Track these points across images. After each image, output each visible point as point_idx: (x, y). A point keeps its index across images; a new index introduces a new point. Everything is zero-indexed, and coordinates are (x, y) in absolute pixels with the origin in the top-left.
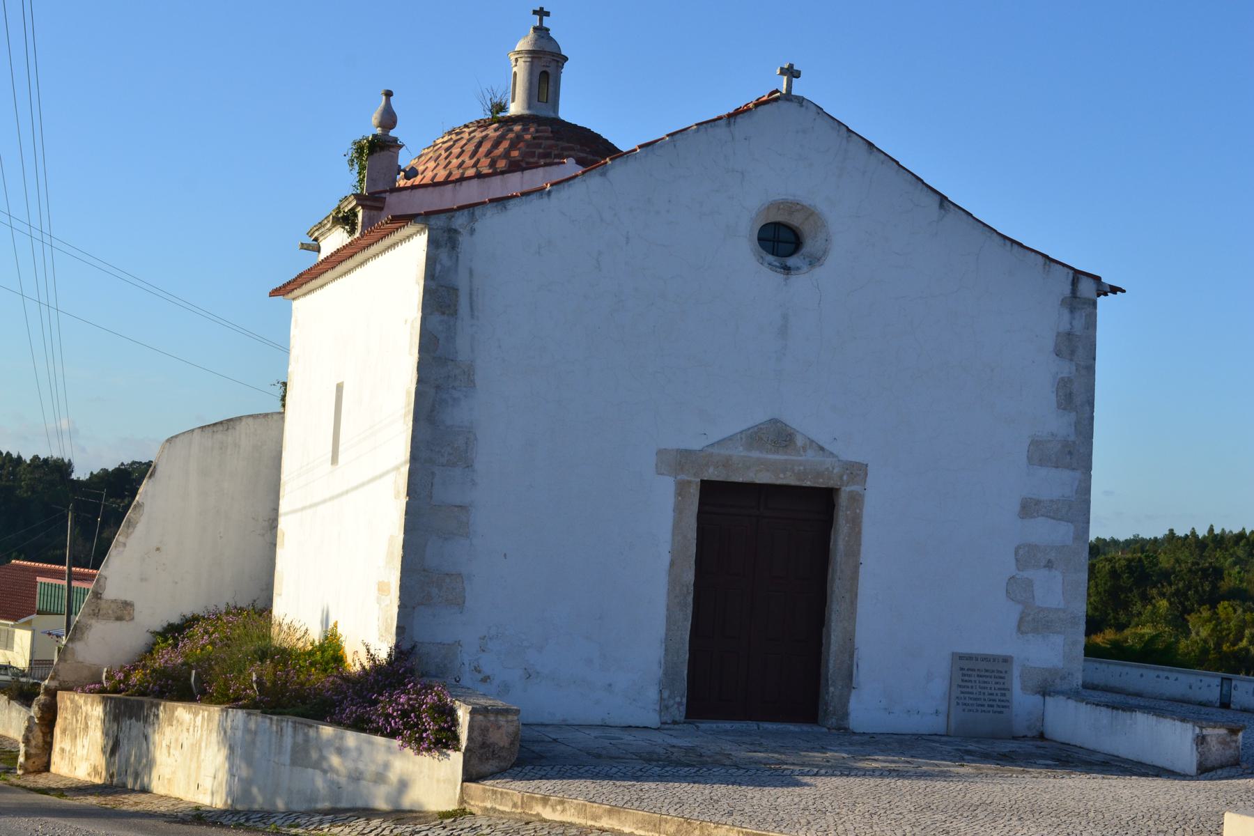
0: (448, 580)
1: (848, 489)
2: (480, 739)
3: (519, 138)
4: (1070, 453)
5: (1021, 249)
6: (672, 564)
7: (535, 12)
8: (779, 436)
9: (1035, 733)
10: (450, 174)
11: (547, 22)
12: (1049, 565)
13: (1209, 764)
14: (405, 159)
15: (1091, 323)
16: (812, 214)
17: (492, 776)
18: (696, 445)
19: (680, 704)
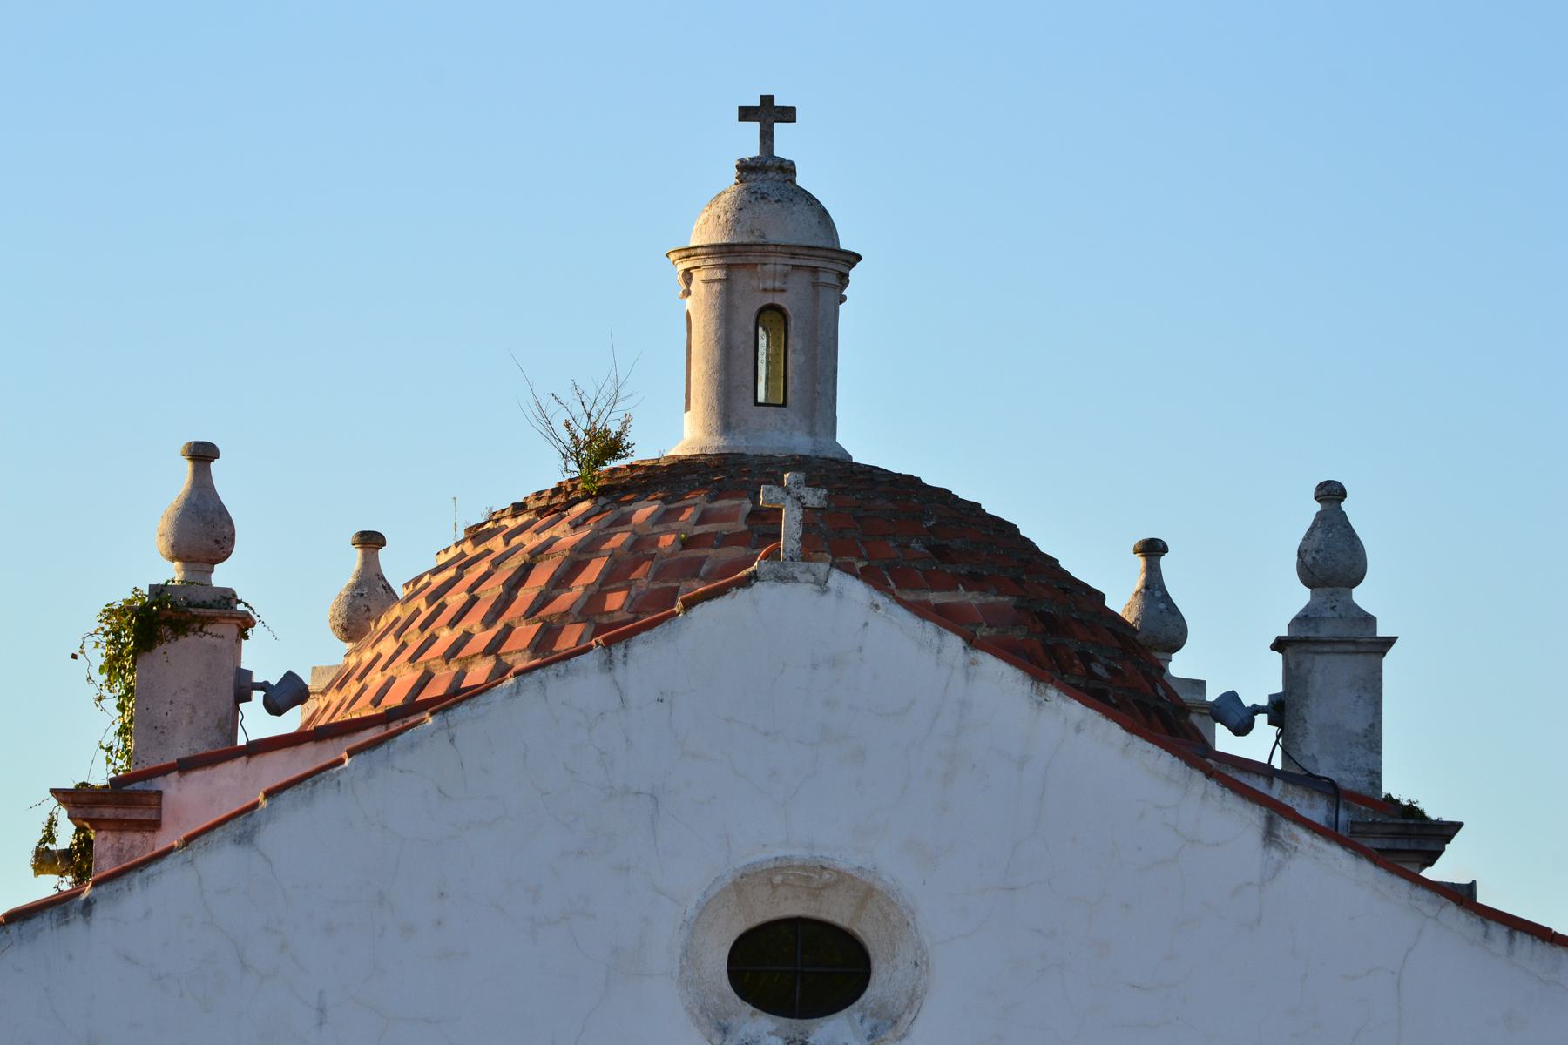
3: (641, 545)
5: (1542, 949)
7: (746, 114)
10: (426, 678)
11: (786, 142)
14: (262, 658)
16: (870, 891)
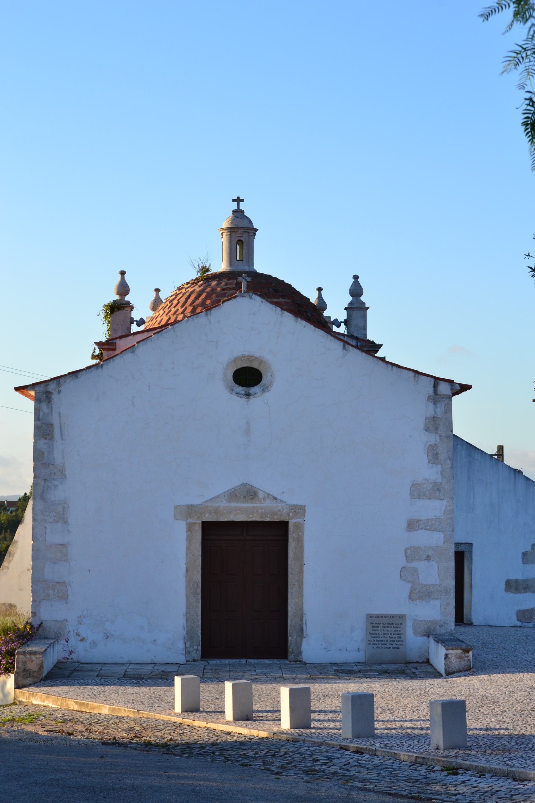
0: (58, 586)
1: (293, 521)
2: (22, 667)
3: (213, 290)
4: (439, 490)
6: (187, 570)
7: (234, 200)
8: (249, 493)
9: (424, 659)
10: (170, 318)
11: (242, 206)
12: (428, 558)
13: (451, 670)
14: (136, 315)
15: (449, 409)
16: (262, 361)
17: (29, 685)
18: (198, 501)
19: (197, 650)
